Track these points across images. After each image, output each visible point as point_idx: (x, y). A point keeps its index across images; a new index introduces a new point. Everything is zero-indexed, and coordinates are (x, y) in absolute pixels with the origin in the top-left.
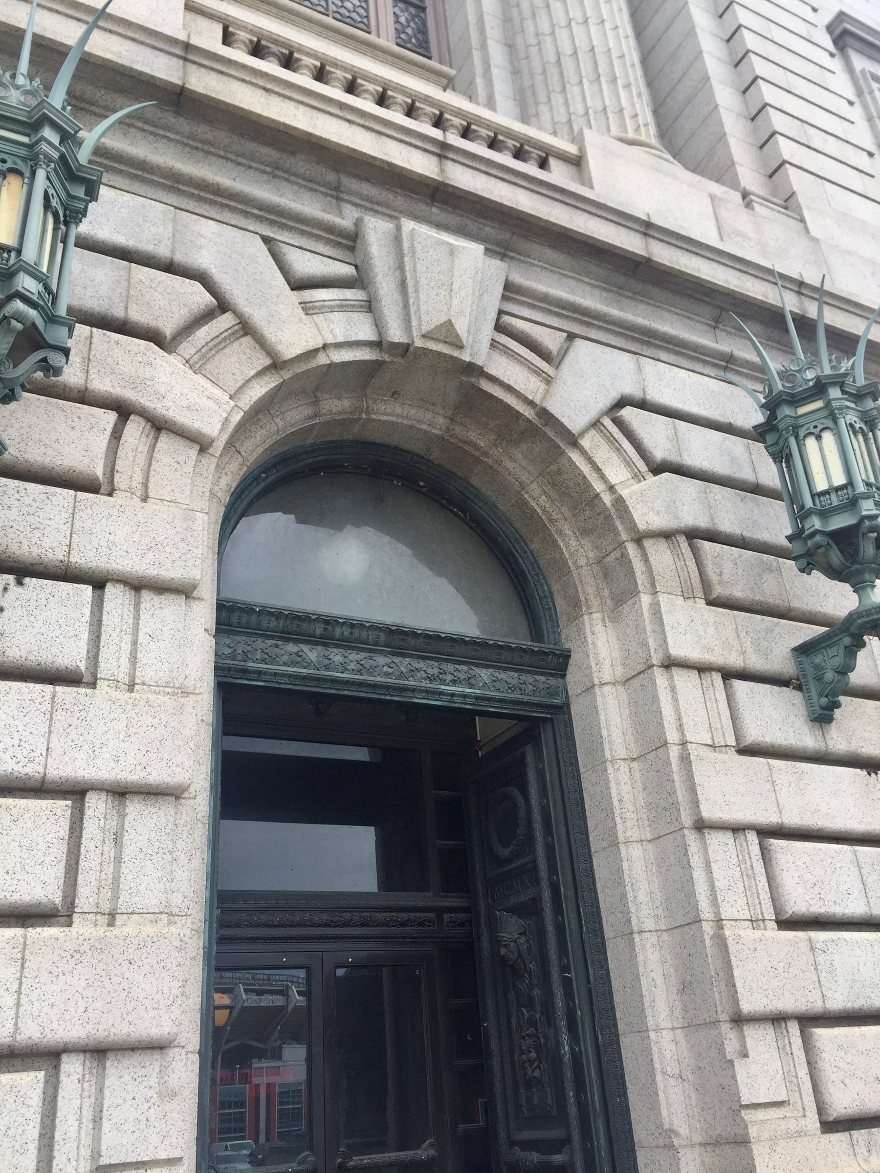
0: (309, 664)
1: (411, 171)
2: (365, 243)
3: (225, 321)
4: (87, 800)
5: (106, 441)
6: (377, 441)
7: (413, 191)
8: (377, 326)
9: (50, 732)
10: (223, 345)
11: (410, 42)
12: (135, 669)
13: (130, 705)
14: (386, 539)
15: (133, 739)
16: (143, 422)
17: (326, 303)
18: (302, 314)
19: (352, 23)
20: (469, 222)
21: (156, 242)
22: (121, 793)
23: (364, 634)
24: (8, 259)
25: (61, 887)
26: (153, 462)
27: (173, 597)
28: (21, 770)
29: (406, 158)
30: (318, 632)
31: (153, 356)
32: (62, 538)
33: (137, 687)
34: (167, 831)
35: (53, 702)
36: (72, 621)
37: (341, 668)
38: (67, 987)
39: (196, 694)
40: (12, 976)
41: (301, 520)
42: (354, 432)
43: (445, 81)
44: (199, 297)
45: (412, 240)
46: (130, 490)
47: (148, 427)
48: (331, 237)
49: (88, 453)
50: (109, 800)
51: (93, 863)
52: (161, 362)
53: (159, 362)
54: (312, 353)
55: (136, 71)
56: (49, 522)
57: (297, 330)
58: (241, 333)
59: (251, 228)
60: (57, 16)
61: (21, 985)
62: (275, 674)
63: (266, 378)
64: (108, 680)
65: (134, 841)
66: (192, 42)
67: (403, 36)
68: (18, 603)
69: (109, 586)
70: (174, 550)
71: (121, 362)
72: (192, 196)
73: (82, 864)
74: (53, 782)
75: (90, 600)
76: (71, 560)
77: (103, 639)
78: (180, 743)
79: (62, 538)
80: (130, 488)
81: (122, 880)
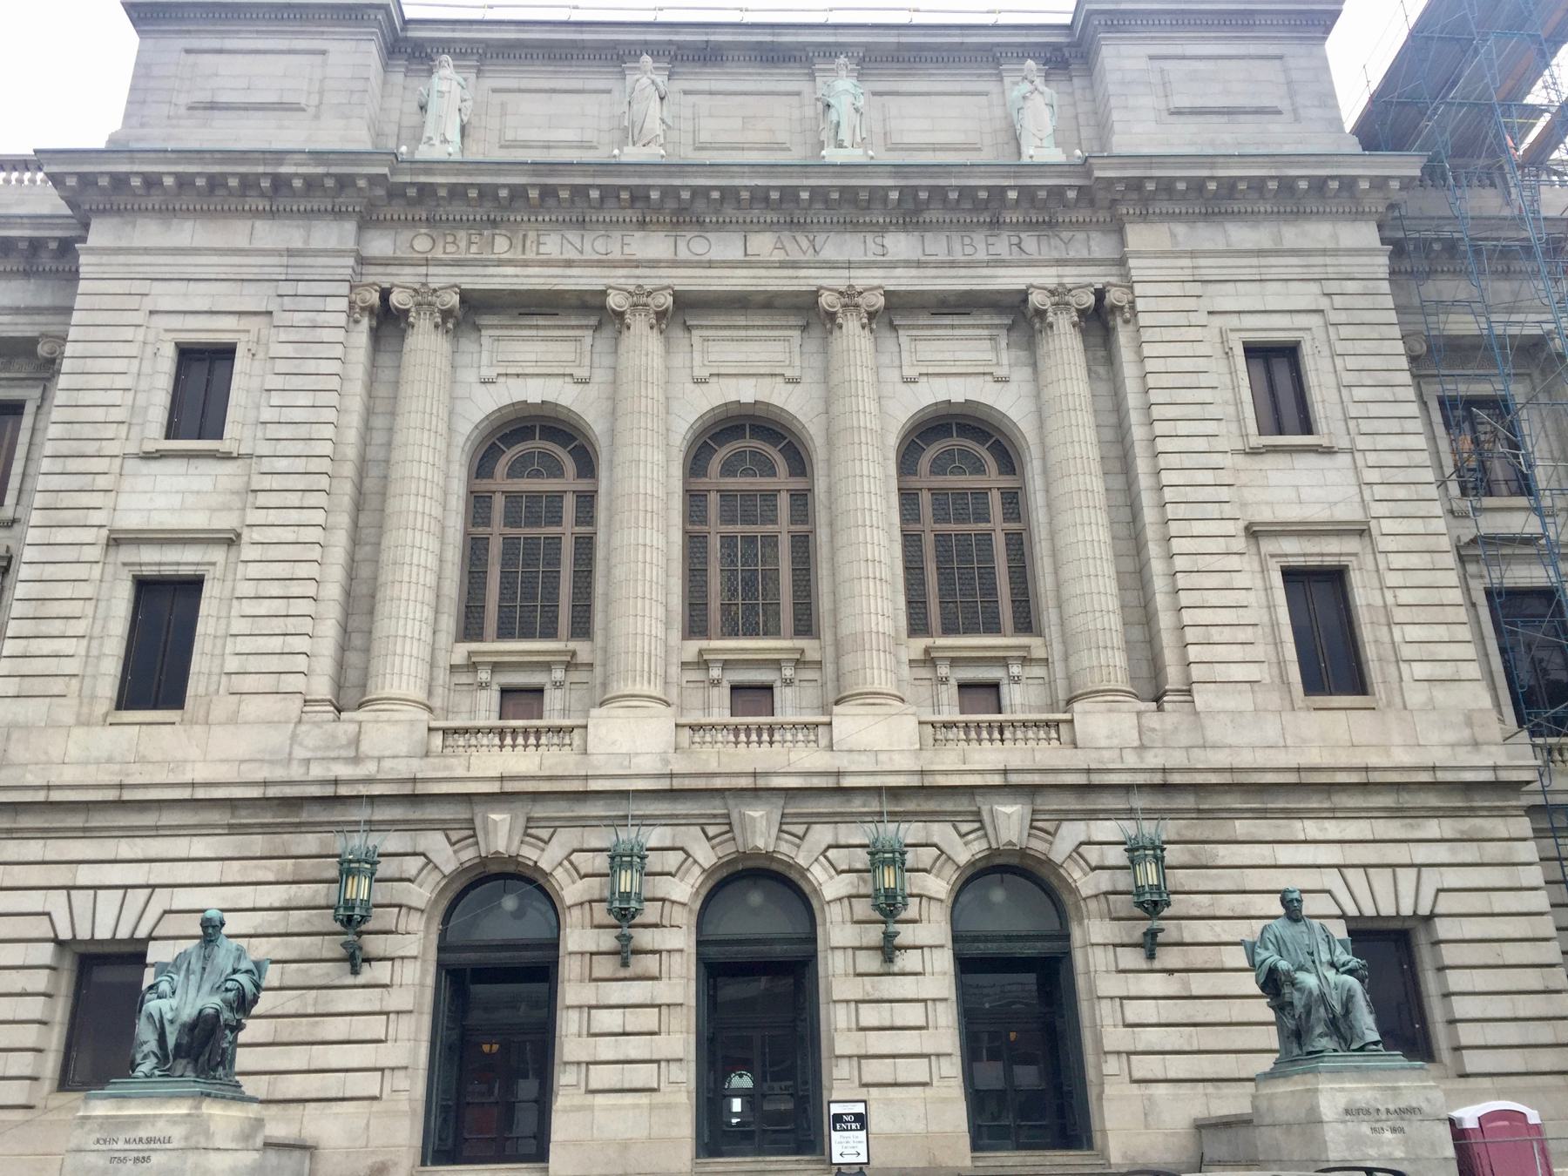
22: (934, 1000)
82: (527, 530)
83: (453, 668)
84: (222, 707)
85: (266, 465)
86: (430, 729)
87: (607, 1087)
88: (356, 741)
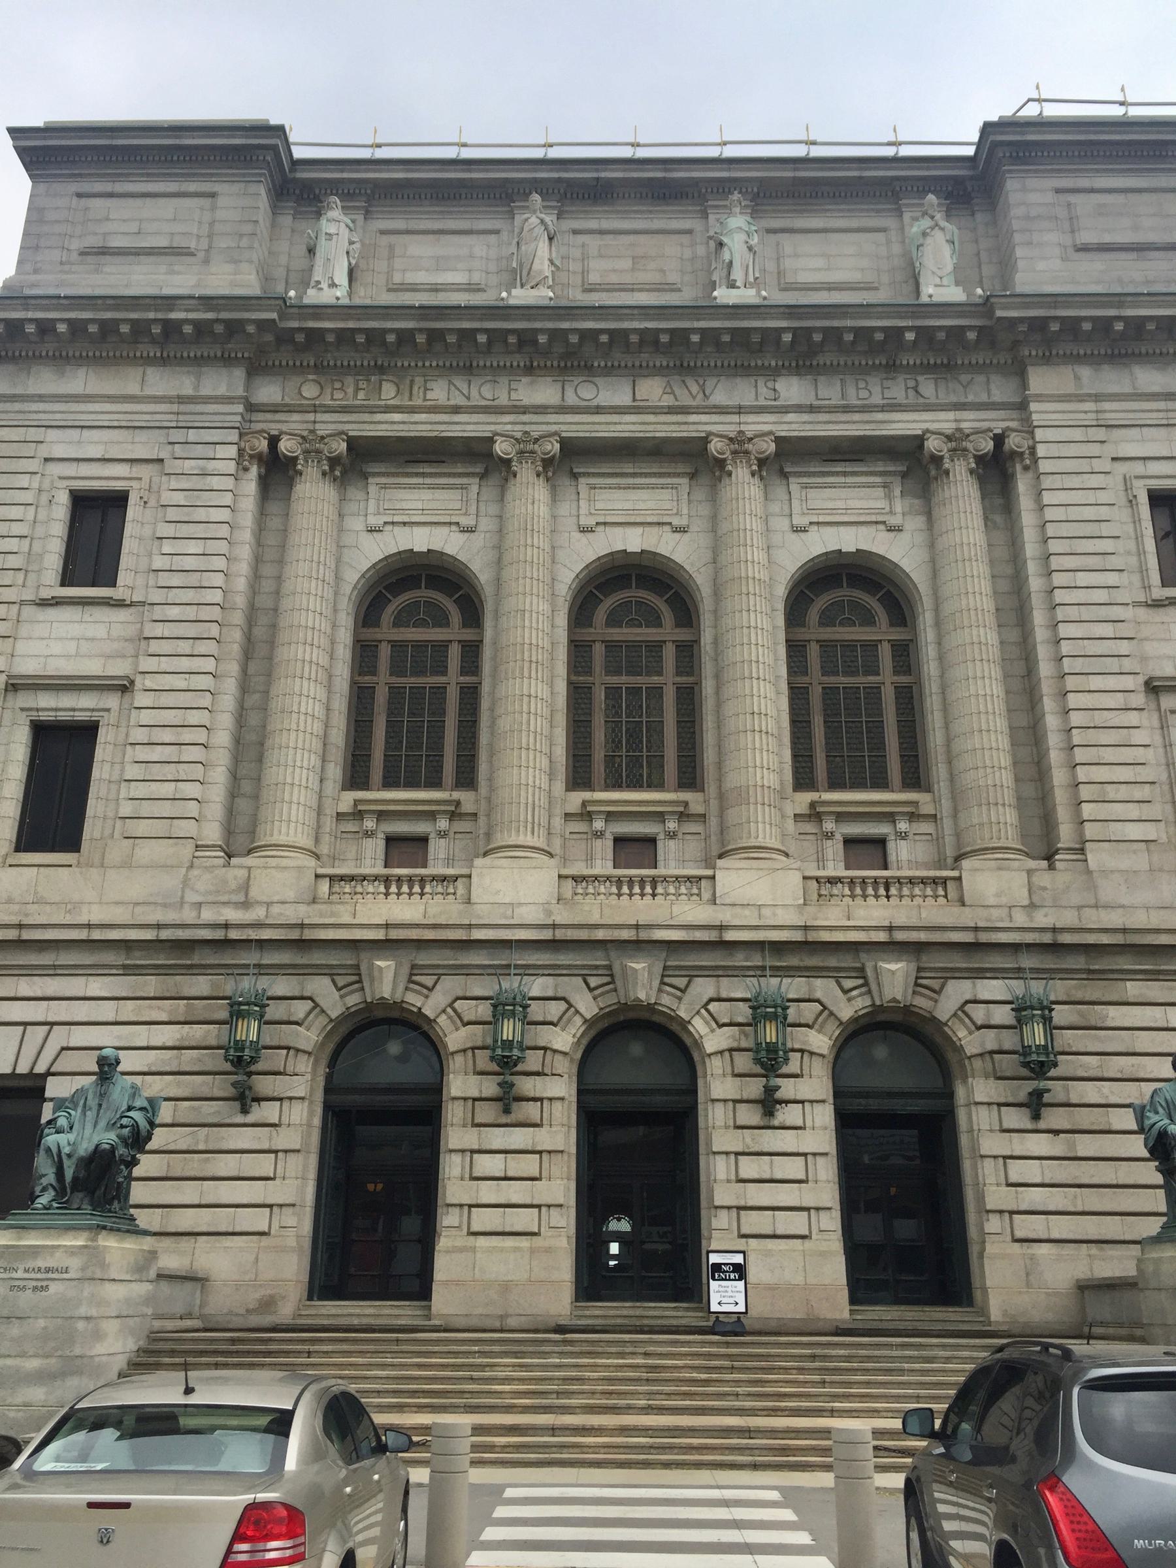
22: (814, 1154)
82: (413, 680)
83: (340, 816)
84: (117, 850)
85: (158, 612)
86: (317, 876)
87: (488, 1229)
88: (246, 886)
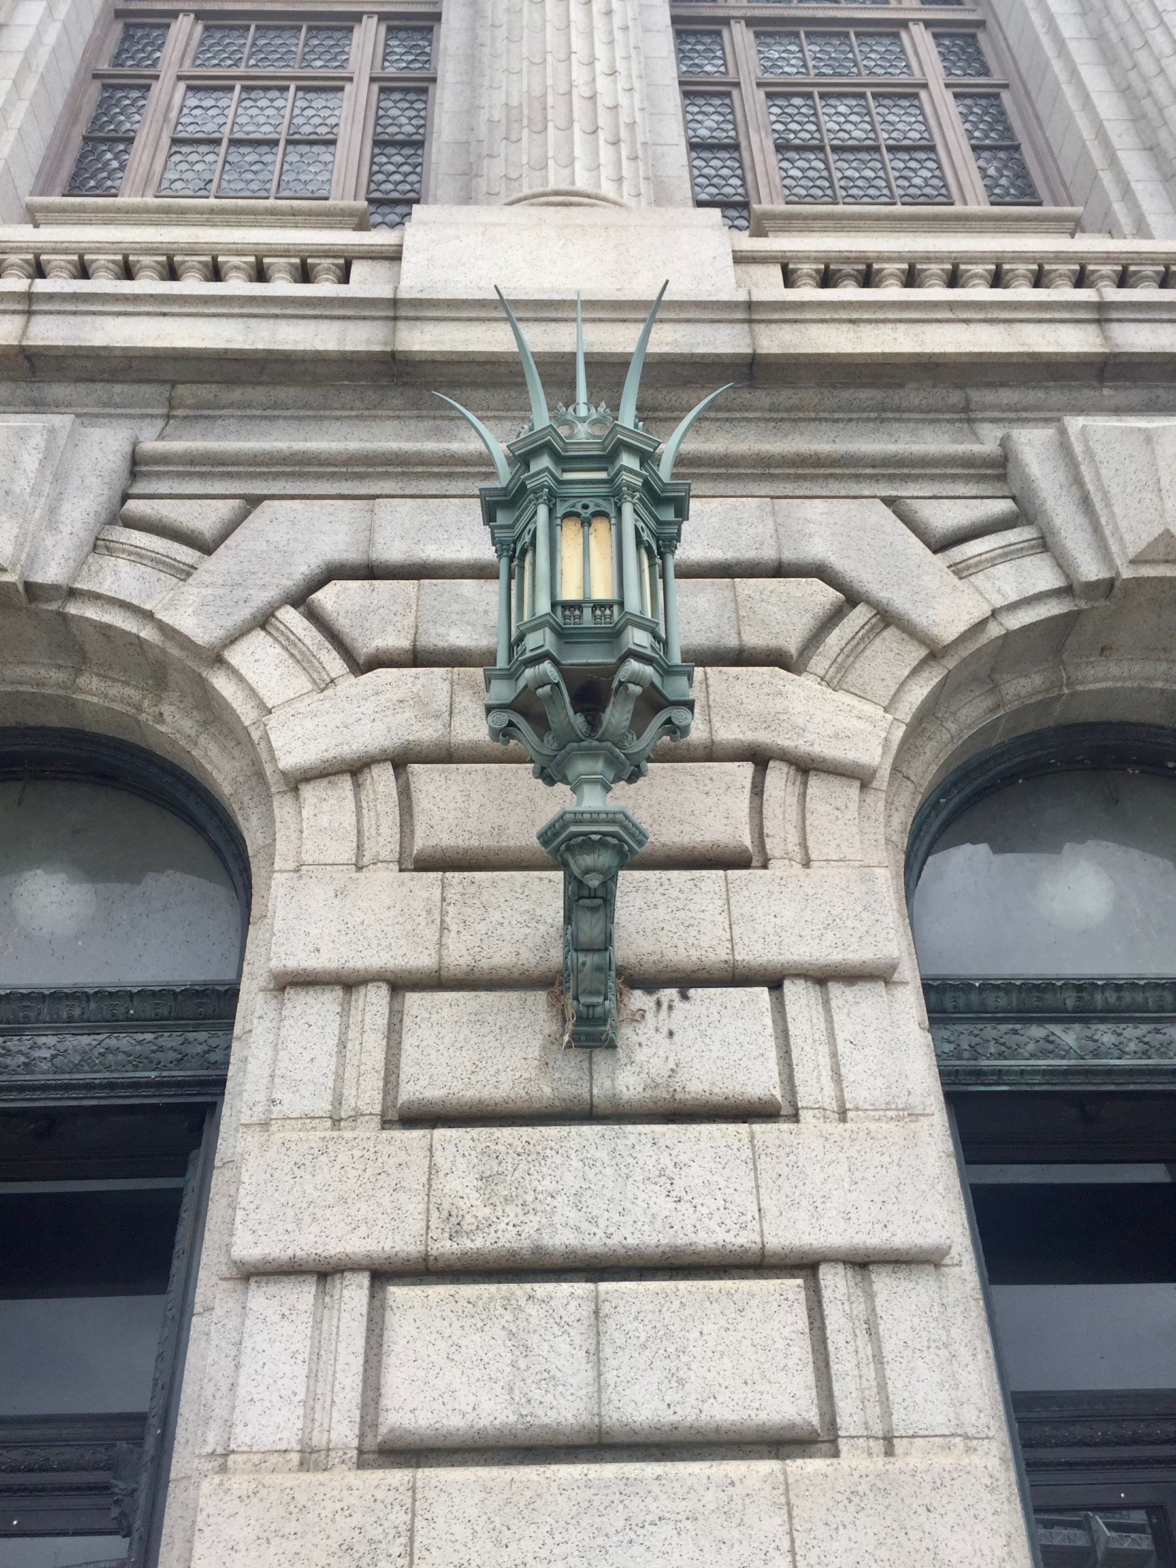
0: (1067, 1052)
1: (1064, 354)
2: (1021, 466)
3: (860, 616)
4: (821, 1277)
5: (747, 801)
6: (1092, 719)
7: (1074, 378)
8: (1060, 566)
9: (757, 1187)
10: (862, 647)
11: (1009, 194)
12: (842, 1090)
13: (848, 1140)
14: (1135, 854)
15: (861, 1186)
16: (785, 768)
17: (983, 557)
18: (955, 580)
19: (928, 200)
20: (1160, 392)
21: (757, 545)
23: (1139, 998)
24: (611, 616)
25: (815, 1402)
26: (808, 815)
27: (869, 986)
28: (733, 1240)
29: (1052, 341)
30: (1070, 1003)
31: (781, 682)
32: (720, 932)
33: (850, 1114)
34: (935, 1316)
35: (753, 1146)
36: (754, 1037)
37: (1116, 1053)
38: (852, 1545)
39: (927, 1115)
40: (780, 1529)
41: (997, 849)
42: (1057, 715)
43: (1071, 225)
44: (823, 595)
45: (1086, 442)
46: (787, 856)
47: (792, 772)
48: (972, 471)
49: (730, 821)
50: (849, 1274)
51: (848, 1364)
52: (791, 689)
53: (790, 688)
54: (981, 625)
55: (698, 355)
56: (702, 915)
57: (950, 605)
58: (882, 625)
59: (866, 493)
60: (602, 325)
61: (793, 1541)
62: (1022, 1072)
63: (925, 674)
64: (812, 1109)
65: (894, 1331)
66: (754, 299)
67: (997, 191)
68: (687, 1023)
69: (787, 984)
70: (857, 924)
71: (745, 700)
72: (787, 478)
73: (834, 1367)
74: (775, 1254)
75: (769, 1006)
76: (737, 957)
77: (794, 1056)
78: (924, 1187)
79: (720, 932)
80: (787, 853)
81: (890, 1388)
